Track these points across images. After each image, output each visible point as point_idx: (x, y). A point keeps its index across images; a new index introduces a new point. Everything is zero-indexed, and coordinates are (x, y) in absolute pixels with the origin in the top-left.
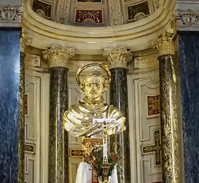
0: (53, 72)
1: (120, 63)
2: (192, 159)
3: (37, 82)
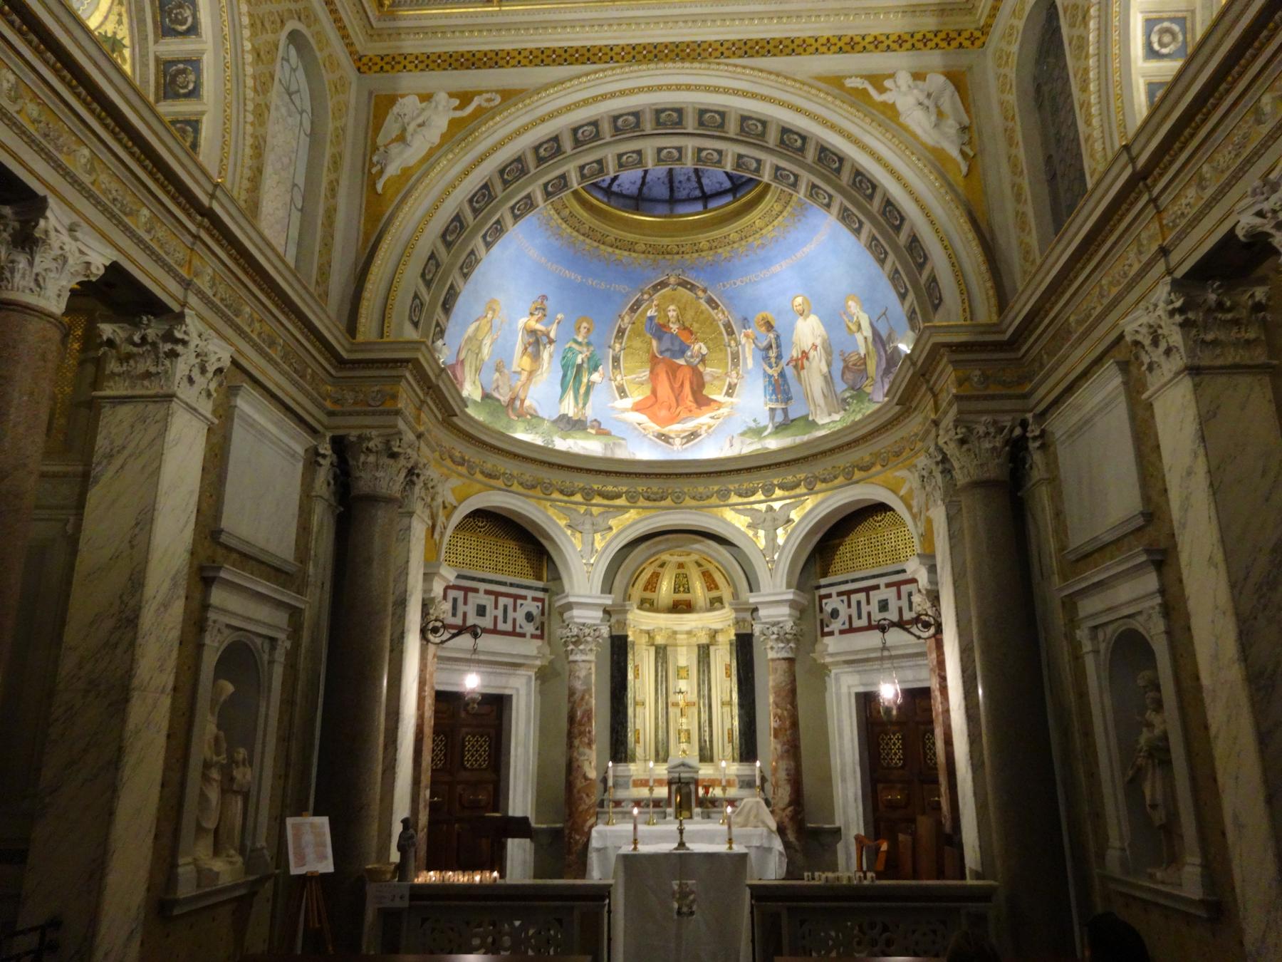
1: (704, 640)
3: (645, 654)
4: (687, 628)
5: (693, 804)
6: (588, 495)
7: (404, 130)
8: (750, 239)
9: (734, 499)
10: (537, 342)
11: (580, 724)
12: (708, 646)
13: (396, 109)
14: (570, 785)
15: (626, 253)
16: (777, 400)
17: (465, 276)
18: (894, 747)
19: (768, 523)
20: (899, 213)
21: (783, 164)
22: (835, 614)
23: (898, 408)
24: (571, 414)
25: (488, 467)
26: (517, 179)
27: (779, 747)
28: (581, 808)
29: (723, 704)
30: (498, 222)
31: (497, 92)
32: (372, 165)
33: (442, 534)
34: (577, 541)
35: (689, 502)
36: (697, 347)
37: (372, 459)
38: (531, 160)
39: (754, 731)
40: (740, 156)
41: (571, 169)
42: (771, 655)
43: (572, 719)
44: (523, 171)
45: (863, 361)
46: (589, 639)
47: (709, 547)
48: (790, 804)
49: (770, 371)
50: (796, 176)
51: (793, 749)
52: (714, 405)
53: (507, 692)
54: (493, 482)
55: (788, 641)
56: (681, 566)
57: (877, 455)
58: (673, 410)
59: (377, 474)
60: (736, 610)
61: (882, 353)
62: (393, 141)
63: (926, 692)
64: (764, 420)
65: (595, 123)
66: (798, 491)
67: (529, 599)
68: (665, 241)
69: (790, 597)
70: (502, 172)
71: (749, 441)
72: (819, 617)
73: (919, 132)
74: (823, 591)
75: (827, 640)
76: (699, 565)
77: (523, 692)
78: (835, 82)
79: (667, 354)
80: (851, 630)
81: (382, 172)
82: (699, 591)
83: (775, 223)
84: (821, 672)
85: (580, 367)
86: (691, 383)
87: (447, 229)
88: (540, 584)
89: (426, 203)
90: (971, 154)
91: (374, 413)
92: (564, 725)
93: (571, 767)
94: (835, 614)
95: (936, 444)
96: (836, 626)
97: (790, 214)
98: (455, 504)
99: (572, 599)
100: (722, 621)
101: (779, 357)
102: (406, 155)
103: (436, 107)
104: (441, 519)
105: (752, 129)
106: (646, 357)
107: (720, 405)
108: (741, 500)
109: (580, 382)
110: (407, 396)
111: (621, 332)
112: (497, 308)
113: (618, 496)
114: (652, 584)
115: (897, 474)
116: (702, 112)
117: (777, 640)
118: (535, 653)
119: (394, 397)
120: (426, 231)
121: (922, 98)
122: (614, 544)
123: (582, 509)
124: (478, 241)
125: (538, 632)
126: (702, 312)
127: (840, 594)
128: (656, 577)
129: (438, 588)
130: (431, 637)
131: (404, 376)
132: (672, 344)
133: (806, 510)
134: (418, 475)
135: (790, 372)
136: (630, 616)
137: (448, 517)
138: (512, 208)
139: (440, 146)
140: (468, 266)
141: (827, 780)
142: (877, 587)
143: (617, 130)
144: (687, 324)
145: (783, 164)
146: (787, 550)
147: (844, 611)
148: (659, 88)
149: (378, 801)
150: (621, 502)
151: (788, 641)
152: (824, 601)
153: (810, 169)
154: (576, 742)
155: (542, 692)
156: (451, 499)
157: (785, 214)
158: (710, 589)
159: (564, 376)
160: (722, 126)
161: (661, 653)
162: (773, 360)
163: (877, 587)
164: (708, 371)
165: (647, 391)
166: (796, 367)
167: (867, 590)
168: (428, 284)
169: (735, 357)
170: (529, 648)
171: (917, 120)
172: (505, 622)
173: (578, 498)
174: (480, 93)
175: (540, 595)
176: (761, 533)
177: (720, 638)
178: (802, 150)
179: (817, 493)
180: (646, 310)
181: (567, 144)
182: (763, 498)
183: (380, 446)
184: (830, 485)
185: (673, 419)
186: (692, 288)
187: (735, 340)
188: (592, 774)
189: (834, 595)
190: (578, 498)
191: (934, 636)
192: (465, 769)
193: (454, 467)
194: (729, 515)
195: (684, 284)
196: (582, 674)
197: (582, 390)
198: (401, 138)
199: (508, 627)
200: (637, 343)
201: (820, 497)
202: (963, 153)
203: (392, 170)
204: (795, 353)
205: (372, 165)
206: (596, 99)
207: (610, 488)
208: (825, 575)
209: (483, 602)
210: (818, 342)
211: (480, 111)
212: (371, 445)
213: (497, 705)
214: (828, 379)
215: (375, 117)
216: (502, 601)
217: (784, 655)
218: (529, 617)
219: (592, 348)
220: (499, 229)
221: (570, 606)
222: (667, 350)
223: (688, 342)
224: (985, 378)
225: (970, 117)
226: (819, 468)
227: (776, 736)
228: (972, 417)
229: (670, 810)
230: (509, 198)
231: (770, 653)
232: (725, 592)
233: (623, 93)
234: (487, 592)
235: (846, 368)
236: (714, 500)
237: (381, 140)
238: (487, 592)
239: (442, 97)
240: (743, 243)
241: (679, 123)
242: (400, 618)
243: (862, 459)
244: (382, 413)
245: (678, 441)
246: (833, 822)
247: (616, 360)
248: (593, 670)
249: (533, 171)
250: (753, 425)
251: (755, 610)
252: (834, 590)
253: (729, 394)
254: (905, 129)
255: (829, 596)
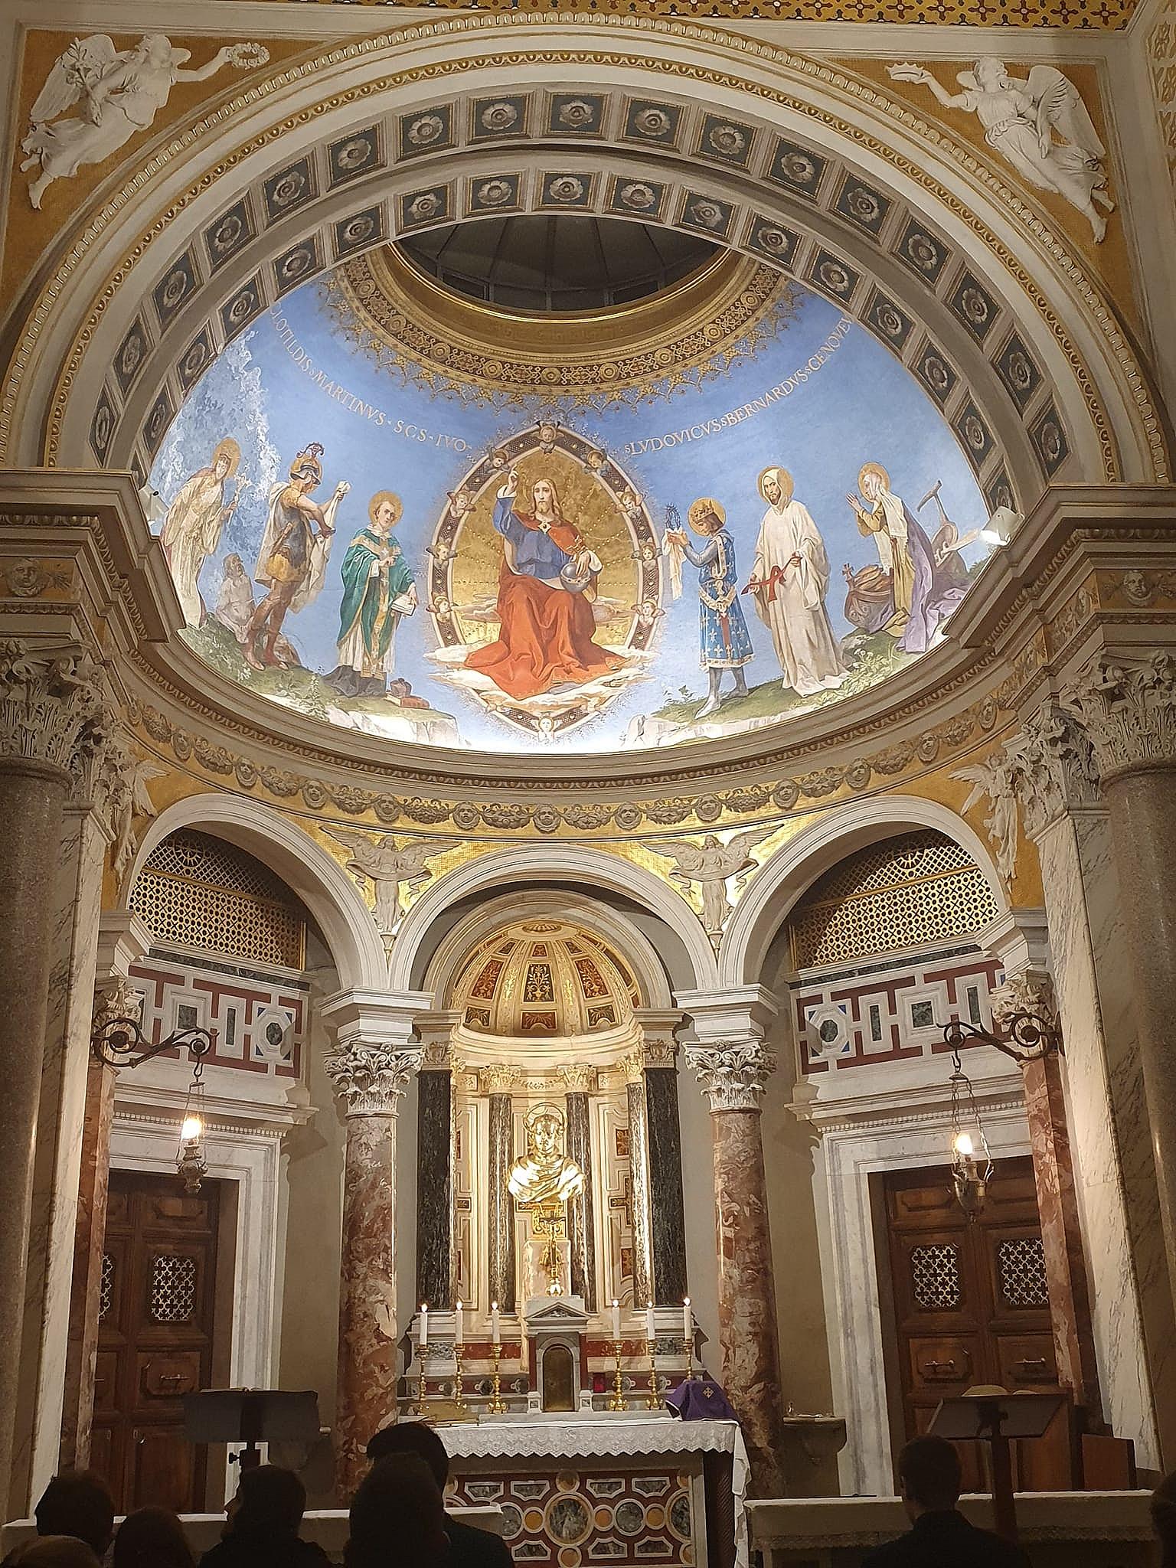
0: (493, 1100)
1: (579, 1086)
2: (663, 1239)
4: (546, 1064)
5: (577, 1383)
6: (388, 812)
7: (85, 95)
8: (692, 362)
9: (648, 827)
10: (301, 534)
11: (370, 1233)
12: (586, 1096)
13: (68, 59)
14: (347, 1350)
15: (467, 377)
16: (724, 656)
17: (188, 382)
18: (940, 1273)
19: (711, 869)
20: (988, 299)
21: (771, 214)
22: (829, 1031)
23: (966, 653)
24: (358, 666)
25: (210, 750)
26: (295, 205)
27: (736, 1272)
28: (369, 1395)
29: (613, 1203)
30: (251, 287)
31: (262, 43)
32: (22, 156)
33: (129, 864)
34: (367, 893)
35: (565, 830)
36: (583, 558)
37: (18, 694)
38: (322, 171)
39: (682, 1248)
40: (694, 198)
41: (387, 198)
42: (718, 1103)
43: (352, 1225)
44: (307, 193)
45: (889, 581)
46: (387, 1073)
47: (597, 913)
48: (757, 1379)
49: (712, 604)
50: (793, 238)
51: (760, 1278)
52: (611, 662)
53: (230, 1175)
54: (219, 778)
55: (749, 1078)
56: (540, 950)
57: (917, 743)
58: (537, 670)
59: (27, 725)
60: (646, 1026)
61: (926, 565)
62: (62, 116)
63: (1023, 1166)
64: (700, 688)
65: (443, 113)
66: (763, 812)
67: (275, 1000)
68: (539, 358)
69: (755, 997)
70: (270, 186)
71: (673, 725)
72: (798, 1037)
73: (1020, 163)
74: (805, 992)
75: (813, 1078)
76: (573, 948)
77: (258, 1174)
78: (871, 70)
79: (530, 570)
80: (862, 1059)
81: (40, 169)
82: (570, 1000)
83: (740, 332)
84: (804, 1136)
85: (375, 581)
86: (571, 622)
87: (165, 281)
88: (294, 974)
89: (130, 229)
90: (1110, 206)
91: (21, 609)
92: (337, 1237)
93: (351, 1315)
94: (829, 1031)
95: (1055, 708)
96: (830, 1052)
97: (772, 314)
98: (153, 811)
99: (357, 999)
100: (616, 1050)
101: (730, 578)
102: (89, 141)
103: (146, 60)
104: (129, 835)
105: (725, 145)
106: (495, 574)
107: (621, 661)
108: (659, 828)
109: (375, 612)
110: (87, 581)
111: (450, 525)
112: (235, 458)
113: (441, 817)
114: (486, 985)
115: (958, 774)
116: (638, 106)
117: (728, 1076)
118: (283, 1101)
119: (63, 581)
120: (128, 281)
121: (1025, 107)
122: (433, 902)
123: (377, 837)
124: (214, 319)
125: (290, 1064)
126: (595, 495)
127: (836, 996)
128: (495, 967)
129: (121, 964)
130: (108, 1053)
131: (84, 543)
132: (540, 552)
133: (785, 840)
134: (98, 739)
135: (749, 604)
136: (453, 1036)
137: (140, 834)
138: (279, 263)
139: (153, 131)
140: (195, 363)
141: (818, 1335)
142: (909, 981)
143: (481, 132)
144: (567, 516)
145: (771, 214)
146: (744, 914)
147: (845, 1026)
148: (565, 56)
149: (17, 1364)
150: (447, 827)
151: (749, 1078)
152: (807, 1009)
153: (821, 223)
154: (361, 1269)
155: (292, 1177)
156: (144, 800)
157: (760, 313)
158: (589, 993)
159: (348, 597)
160: (668, 138)
161: (500, 1107)
162: (719, 585)
163: (909, 981)
164: (600, 601)
165: (493, 631)
166: (759, 595)
167: (890, 987)
168: (125, 381)
169: (651, 580)
170: (274, 1090)
171: (1019, 145)
172: (230, 1041)
173: (370, 817)
174: (231, 42)
175: (294, 994)
176: (697, 887)
177: (606, 1083)
178: (811, 186)
179: (800, 813)
180: (496, 487)
181: (390, 149)
182: (699, 824)
183: (35, 671)
184: (824, 800)
185: (536, 688)
186: (580, 449)
187: (652, 547)
188: (391, 1330)
189: (827, 997)
190: (370, 817)
191: (1043, 1055)
192: (155, 1322)
193: (151, 742)
194: (641, 855)
195: (566, 441)
196: (374, 1139)
197: (378, 626)
198: (81, 111)
199: (236, 1051)
200: (477, 547)
201: (805, 821)
202: (1094, 201)
203: (61, 167)
204: (760, 572)
205: (22, 156)
206: (447, 68)
207: (426, 802)
208: (807, 962)
209: (191, 1002)
210: (803, 550)
211: (229, 75)
212: (17, 667)
213: (218, 1195)
214: (820, 616)
215: (28, 69)
216: (226, 1001)
217: (741, 1103)
218: (274, 1033)
219: (397, 550)
220: (251, 304)
221: (353, 1012)
222: (530, 562)
223: (567, 549)
224: (1149, 585)
225: (1105, 145)
226: (801, 772)
227: (728, 1254)
228: (1129, 652)
229: (535, 1395)
230: (272, 243)
231: (714, 1104)
232: (619, 997)
233: (497, 60)
234: (199, 984)
235: (854, 594)
236: (611, 828)
237: (37, 114)
238: (199, 984)
239: (159, 43)
240: (678, 368)
241: (593, 127)
242: (61, 1010)
243: (885, 752)
244: (37, 610)
245: (546, 724)
246: (828, 1409)
247: (439, 574)
248: (393, 1131)
249: (324, 195)
250: (679, 697)
251: (686, 1020)
252: (826, 990)
253: (638, 642)
254: (996, 156)
255: (817, 999)
